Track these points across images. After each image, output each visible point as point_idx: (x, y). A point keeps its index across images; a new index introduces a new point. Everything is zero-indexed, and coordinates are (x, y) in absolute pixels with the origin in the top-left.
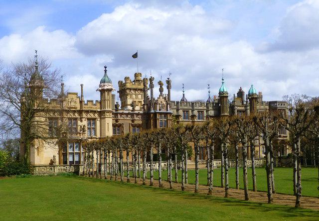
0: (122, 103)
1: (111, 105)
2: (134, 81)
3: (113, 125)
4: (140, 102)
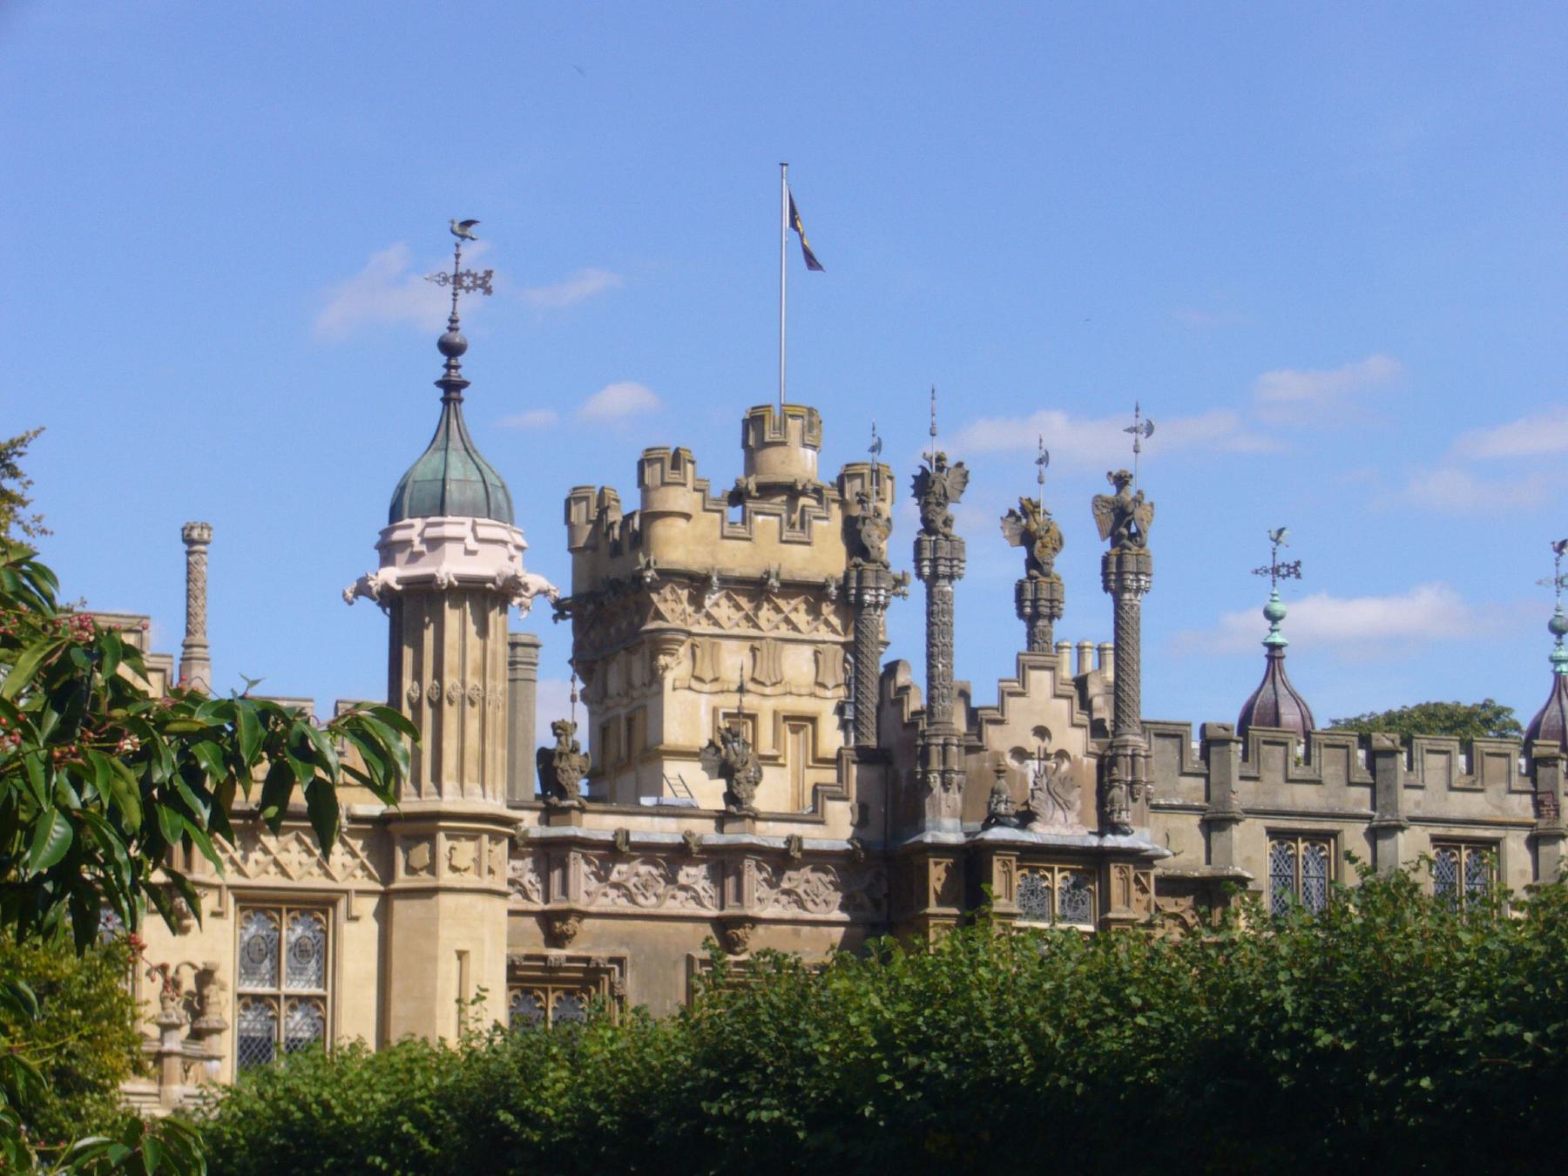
0: (602, 732)
1: (498, 754)
2: (737, 497)
3: (512, 968)
4: (802, 722)
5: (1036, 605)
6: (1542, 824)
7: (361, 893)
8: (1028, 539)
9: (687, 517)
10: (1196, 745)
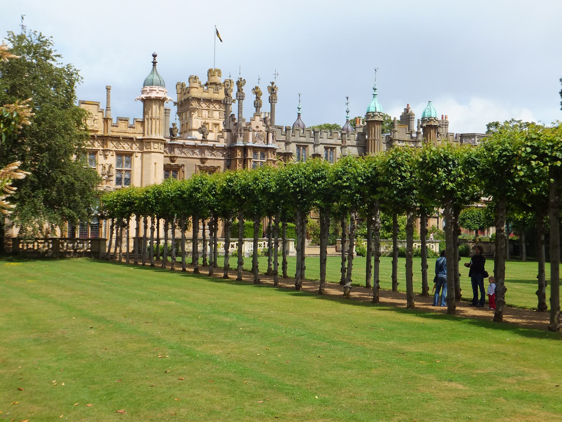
1: (162, 129)
2: (206, 85)
3: (164, 166)
4: (216, 125)
5: (258, 105)
6: (343, 145)
7: (138, 152)
8: (256, 93)
9: (197, 88)
10: (284, 130)
